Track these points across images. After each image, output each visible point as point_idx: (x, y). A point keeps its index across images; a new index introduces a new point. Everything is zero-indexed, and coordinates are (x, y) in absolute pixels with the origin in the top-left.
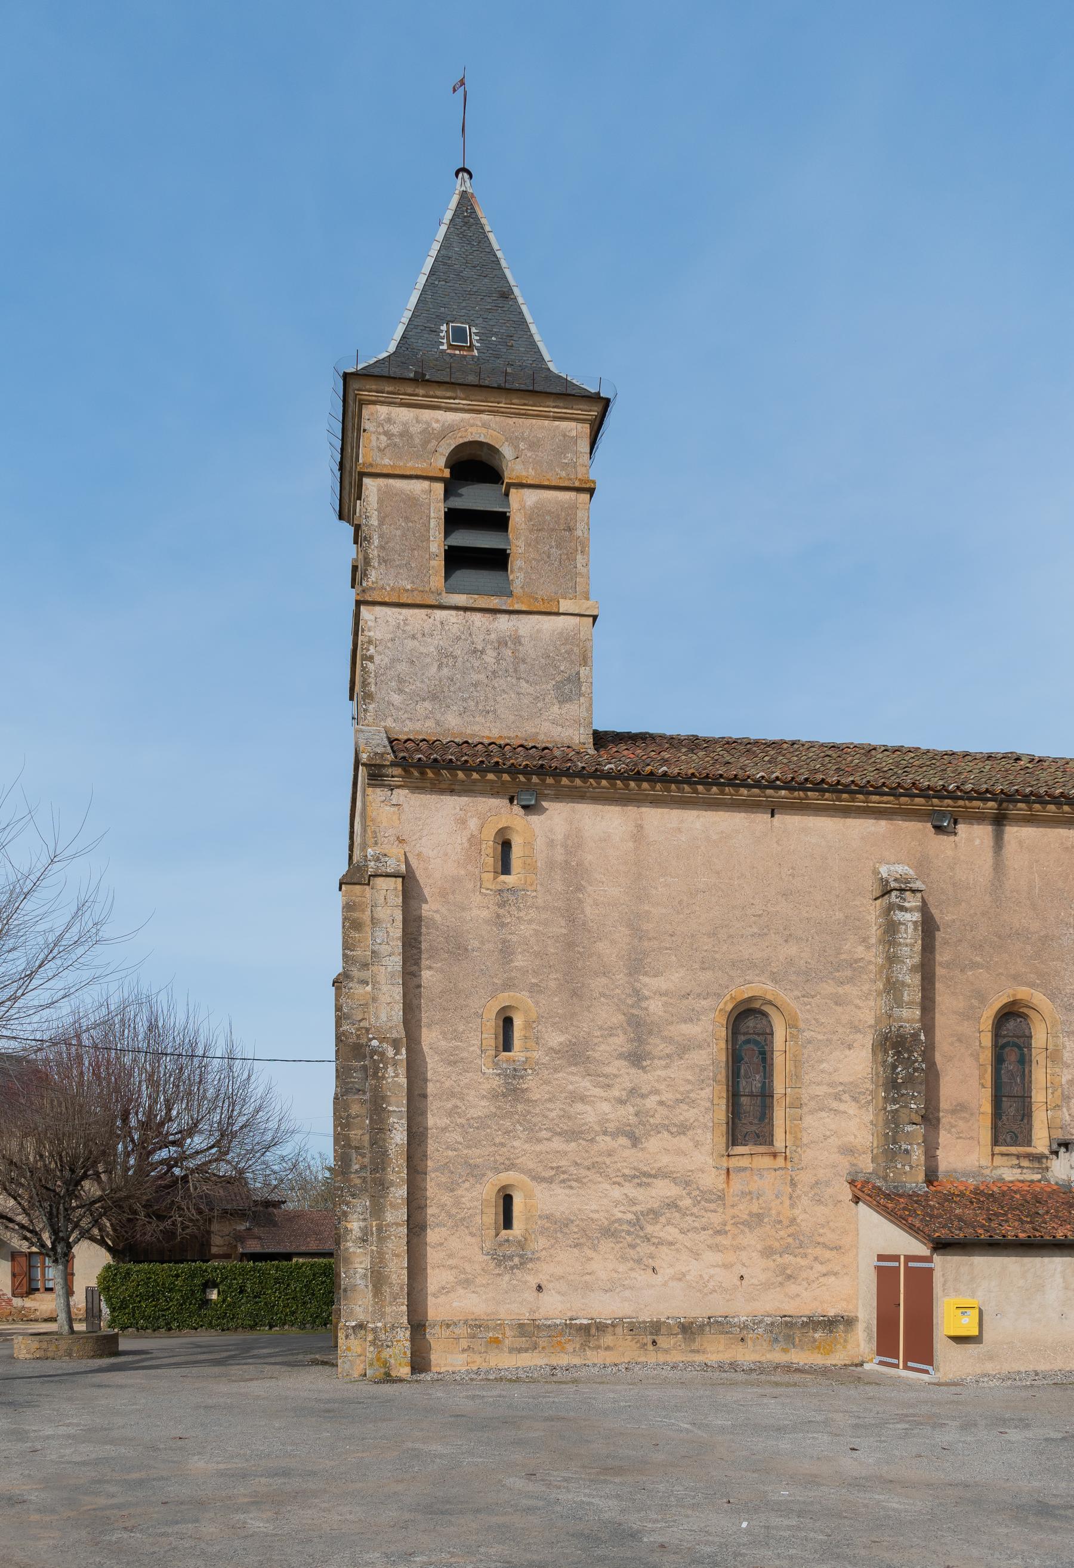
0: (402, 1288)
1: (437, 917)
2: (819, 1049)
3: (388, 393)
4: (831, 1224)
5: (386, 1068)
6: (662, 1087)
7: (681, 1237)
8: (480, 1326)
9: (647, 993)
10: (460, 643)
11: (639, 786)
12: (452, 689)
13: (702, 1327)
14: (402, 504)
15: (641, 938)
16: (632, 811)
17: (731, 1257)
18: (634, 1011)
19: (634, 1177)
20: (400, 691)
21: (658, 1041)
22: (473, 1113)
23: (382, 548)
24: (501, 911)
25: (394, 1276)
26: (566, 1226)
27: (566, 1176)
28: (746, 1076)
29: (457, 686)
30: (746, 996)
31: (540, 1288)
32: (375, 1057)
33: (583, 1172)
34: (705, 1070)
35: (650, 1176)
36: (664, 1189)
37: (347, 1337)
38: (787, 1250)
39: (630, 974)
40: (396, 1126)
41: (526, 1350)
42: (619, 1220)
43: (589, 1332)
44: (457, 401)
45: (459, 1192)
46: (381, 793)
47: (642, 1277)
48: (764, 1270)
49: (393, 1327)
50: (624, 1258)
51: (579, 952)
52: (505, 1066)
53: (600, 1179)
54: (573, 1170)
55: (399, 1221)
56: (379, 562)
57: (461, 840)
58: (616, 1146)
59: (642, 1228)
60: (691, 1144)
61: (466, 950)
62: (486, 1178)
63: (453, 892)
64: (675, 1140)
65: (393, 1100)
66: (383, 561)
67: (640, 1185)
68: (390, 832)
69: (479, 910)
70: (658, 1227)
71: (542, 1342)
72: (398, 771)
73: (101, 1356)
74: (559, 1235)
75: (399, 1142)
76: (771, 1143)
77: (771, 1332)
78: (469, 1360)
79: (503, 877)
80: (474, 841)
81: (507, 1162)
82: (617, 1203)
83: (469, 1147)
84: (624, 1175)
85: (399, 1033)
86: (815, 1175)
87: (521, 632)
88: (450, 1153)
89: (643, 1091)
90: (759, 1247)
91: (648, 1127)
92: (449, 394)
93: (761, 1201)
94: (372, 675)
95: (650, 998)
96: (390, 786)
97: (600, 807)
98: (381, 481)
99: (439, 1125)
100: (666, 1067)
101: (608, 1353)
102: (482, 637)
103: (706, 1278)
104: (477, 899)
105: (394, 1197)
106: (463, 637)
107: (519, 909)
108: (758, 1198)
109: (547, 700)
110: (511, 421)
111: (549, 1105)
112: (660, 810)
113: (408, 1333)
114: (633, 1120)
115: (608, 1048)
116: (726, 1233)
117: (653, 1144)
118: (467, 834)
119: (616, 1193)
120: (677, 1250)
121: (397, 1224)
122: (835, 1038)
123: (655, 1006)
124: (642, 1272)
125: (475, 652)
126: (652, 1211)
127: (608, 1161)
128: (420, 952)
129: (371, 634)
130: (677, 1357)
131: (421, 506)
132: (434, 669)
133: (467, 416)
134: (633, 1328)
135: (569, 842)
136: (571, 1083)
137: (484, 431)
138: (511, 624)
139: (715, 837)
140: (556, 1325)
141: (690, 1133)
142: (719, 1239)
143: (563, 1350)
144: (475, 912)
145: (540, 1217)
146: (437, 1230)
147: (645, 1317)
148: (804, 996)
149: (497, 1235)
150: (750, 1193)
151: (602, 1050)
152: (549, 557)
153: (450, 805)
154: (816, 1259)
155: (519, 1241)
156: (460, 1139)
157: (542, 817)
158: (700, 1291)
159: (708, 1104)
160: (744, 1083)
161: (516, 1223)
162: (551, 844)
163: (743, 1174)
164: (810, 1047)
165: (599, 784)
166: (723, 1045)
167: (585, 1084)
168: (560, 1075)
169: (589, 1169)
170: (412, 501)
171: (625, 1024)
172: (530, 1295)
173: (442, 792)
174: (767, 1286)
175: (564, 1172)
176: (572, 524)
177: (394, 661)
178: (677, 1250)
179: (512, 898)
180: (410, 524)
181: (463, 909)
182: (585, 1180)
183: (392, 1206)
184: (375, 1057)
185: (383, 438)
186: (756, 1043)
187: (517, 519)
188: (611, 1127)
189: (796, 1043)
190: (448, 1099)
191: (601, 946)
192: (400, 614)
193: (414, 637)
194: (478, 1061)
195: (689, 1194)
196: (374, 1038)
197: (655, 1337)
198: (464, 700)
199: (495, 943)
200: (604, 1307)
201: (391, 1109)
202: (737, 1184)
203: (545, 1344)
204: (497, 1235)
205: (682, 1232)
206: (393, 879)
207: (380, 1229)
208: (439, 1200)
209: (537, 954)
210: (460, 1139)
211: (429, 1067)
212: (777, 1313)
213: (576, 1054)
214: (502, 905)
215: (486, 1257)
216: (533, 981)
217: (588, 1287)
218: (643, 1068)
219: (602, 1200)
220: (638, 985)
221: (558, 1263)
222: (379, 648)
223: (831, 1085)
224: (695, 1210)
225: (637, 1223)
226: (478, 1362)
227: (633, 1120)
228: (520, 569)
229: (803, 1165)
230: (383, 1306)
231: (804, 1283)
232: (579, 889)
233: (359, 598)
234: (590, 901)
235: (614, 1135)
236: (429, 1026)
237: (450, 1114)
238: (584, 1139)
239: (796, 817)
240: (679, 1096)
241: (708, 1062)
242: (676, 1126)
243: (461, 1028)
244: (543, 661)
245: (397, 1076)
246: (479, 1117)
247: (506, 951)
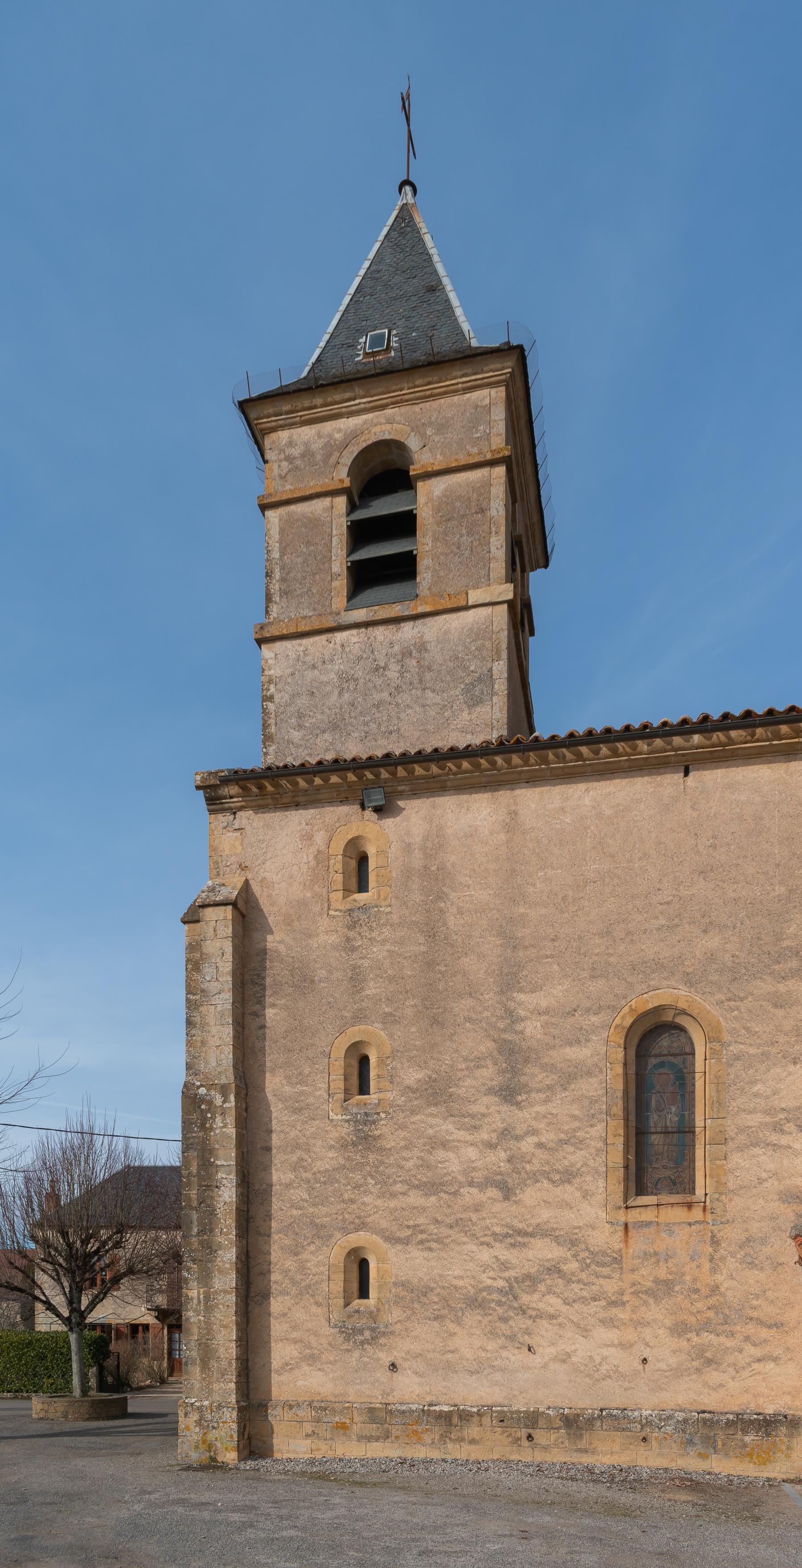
0: (230, 1363)
1: (282, 948)
2: (750, 1066)
3: (287, 413)
4: (769, 1294)
5: (213, 1118)
6: (542, 1126)
7: (564, 1309)
8: (325, 1409)
9: (522, 1013)
10: (362, 663)
11: (508, 762)
12: (353, 715)
13: (591, 1421)
14: (303, 530)
15: (515, 947)
16: (504, 796)
17: (630, 1335)
18: (507, 1036)
19: (507, 1235)
20: (300, 726)
21: (536, 1070)
22: (320, 1166)
23: (283, 580)
24: (352, 934)
25: (222, 1350)
26: (425, 1294)
27: (424, 1236)
28: (659, 1110)
29: (358, 710)
30: (650, 1006)
31: (393, 1366)
32: (203, 1107)
33: (444, 1231)
34: (596, 1101)
35: (526, 1234)
36: (544, 1251)
37: (186, 1415)
38: (706, 1326)
39: (502, 992)
40: (225, 1181)
41: (377, 1439)
42: (488, 1288)
43: (451, 1421)
44: (357, 401)
45: (305, 1256)
46: (223, 819)
47: (516, 1357)
48: (674, 1352)
49: (220, 1407)
50: (493, 1334)
51: (440, 972)
52: (355, 1110)
53: (465, 1239)
54: (433, 1229)
55: (227, 1287)
56: (281, 597)
57: (307, 857)
58: (484, 1199)
59: (516, 1298)
60: (578, 1194)
61: (313, 981)
62: (333, 1240)
63: (298, 919)
64: (558, 1191)
65: (221, 1153)
66: (285, 593)
67: (513, 1245)
68: (233, 859)
69: (327, 935)
70: (536, 1296)
71: (395, 1431)
72: (234, 790)
73: (97, 1419)
74: (416, 1305)
75: (228, 1200)
76: (692, 1191)
77: (684, 1431)
78: (314, 1447)
79: (357, 896)
80: (322, 858)
81: (357, 1221)
82: (485, 1268)
83: (315, 1205)
84: (494, 1234)
85: (228, 1077)
86: (747, 1230)
87: (427, 638)
88: (295, 1212)
89: (518, 1132)
90: (668, 1322)
91: (523, 1175)
92: (347, 395)
93: (670, 1264)
94: (273, 716)
95: (527, 1018)
96: (231, 809)
97: (465, 797)
98: (282, 511)
99: (283, 1181)
100: (546, 1101)
101: (473, 1447)
102: (384, 652)
103: (598, 1359)
104: (324, 923)
105: (223, 1261)
106: (365, 656)
107: (371, 929)
108: (666, 1261)
109: (455, 707)
110: (417, 408)
111: (405, 1154)
112: (538, 790)
113: (235, 1414)
114: (505, 1167)
115: (474, 1083)
116: (623, 1304)
117: (529, 1196)
118: (313, 850)
119: (485, 1255)
120: (560, 1325)
121: (225, 1292)
122: (773, 1050)
123: (533, 1028)
124: (516, 1351)
125: (377, 670)
126: (528, 1276)
127: (474, 1217)
128: (264, 989)
129: (272, 672)
130: (558, 1457)
131: (323, 525)
132: (334, 697)
133: (370, 416)
134: (503, 1418)
135: (429, 844)
136: (431, 1127)
137: (388, 427)
138: (416, 630)
139: (608, 812)
140: (411, 1412)
141: (577, 1180)
142: (614, 1311)
143: (420, 1441)
144: (323, 938)
145: (395, 1284)
146: (280, 1299)
147: (520, 1405)
148: (729, 1000)
149: (347, 1305)
150: (656, 1254)
151: (467, 1086)
152: (459, 548)
153: (296, 821)
154: (747, 1339)
155: (371, 1313)
156: (306, 1196)
157: (398, 819)
158: (589, 1375)
159: (600, 1145)
160: (656, 1117)
161: (373, 1292)
162: (408, 848)
163: (646, 1230)
164: (738, 1065)
165: (459, 766)
166: (619, 1069)
167: (447, 1127)
168: (418, 1117)
169: (451, 1227)
170: (313, 523)
171: (495, 1053)
172: (383, 1375)
173: (286, 807)
174: (678, 1372)
175: (422, 1232)
176: (484, 504)
177: (293, 696)
178: (560, 1325)
179: (363, 917)
180: (312, 548)
181: (310, 936)
182: (447, 1241)
183: (221, 1271)
184: (203, 1107)
185: (285, 464)
186: (672, 1066)
187: (425, 515)
188: (478, 1176)
189: (719, 1060)
190: (293, 1152)
191: (469, 963)
192: (300, 645)
193: (314, 667)
194: (325, 1107)
195: (575, 1256)
196: (202, 1086)
197: (530, 1431)
198: (366, 724)
199: (344, 971)
200: (472, 1392)
201: (218, 1163)
202: (639, 1243)
203: (399, 1433)
204: (347, 1305)
205: (566, 1302)
206: (223, 908)
207: (207, 1298)
208: (283, 1264)
209: (391, 979)
210: (306, 1196)
211: (274, 1115)
212: (693, 1408)
213: (437, 1093)
214: (352, 926)
215: (332, 1330)
216: (387, 1010)
217: (450, 1368)
218: (518, 1104)
219: (468, 1264)
220: (511, 1005)
221: (414, 1338)
222: (279, 686)
223: (767, 1112)
224: (583, 1276)
225: (510, 1292)
226: (323, 1450)
227: (505, 1167)
228: (428, 568)
229: (729, 1216)
230: (210, 1383)
231: (731, 1370)
232: (441, 896)
233: (258, 636)
234: (454, 910)
235: (482, 1186)
236: (273, 1070)
237: (294, 1168)
238: (445, 1192)
239: (719, 771)
240: (562, 1136)
241: (600, 1092)
242: (558, 1172)
243: (307, 1071)
244: (451, 664)
245: (225, 1126)
246: (326, 1171)
247: (357, 979)
